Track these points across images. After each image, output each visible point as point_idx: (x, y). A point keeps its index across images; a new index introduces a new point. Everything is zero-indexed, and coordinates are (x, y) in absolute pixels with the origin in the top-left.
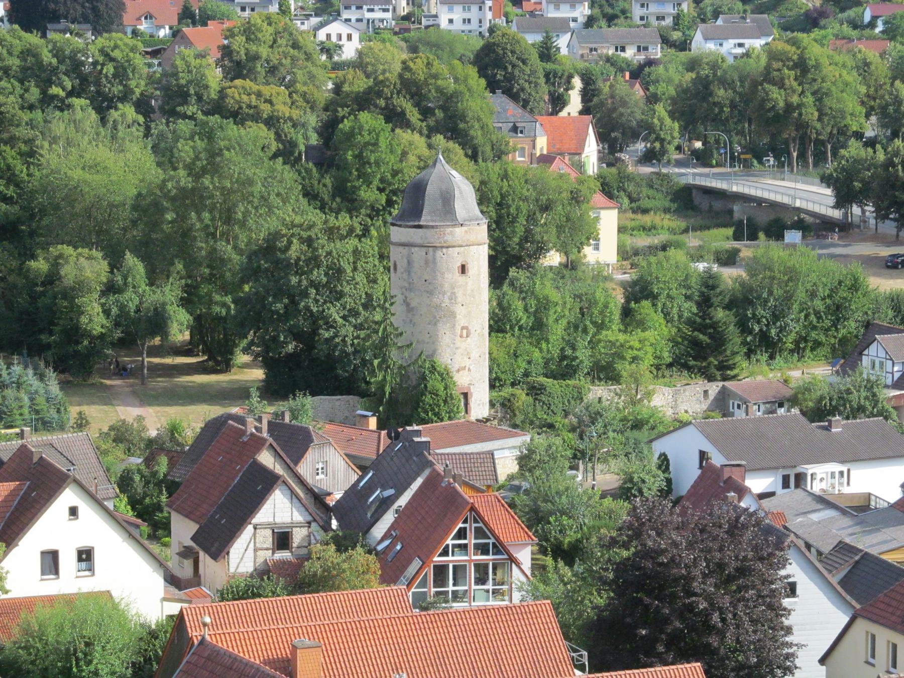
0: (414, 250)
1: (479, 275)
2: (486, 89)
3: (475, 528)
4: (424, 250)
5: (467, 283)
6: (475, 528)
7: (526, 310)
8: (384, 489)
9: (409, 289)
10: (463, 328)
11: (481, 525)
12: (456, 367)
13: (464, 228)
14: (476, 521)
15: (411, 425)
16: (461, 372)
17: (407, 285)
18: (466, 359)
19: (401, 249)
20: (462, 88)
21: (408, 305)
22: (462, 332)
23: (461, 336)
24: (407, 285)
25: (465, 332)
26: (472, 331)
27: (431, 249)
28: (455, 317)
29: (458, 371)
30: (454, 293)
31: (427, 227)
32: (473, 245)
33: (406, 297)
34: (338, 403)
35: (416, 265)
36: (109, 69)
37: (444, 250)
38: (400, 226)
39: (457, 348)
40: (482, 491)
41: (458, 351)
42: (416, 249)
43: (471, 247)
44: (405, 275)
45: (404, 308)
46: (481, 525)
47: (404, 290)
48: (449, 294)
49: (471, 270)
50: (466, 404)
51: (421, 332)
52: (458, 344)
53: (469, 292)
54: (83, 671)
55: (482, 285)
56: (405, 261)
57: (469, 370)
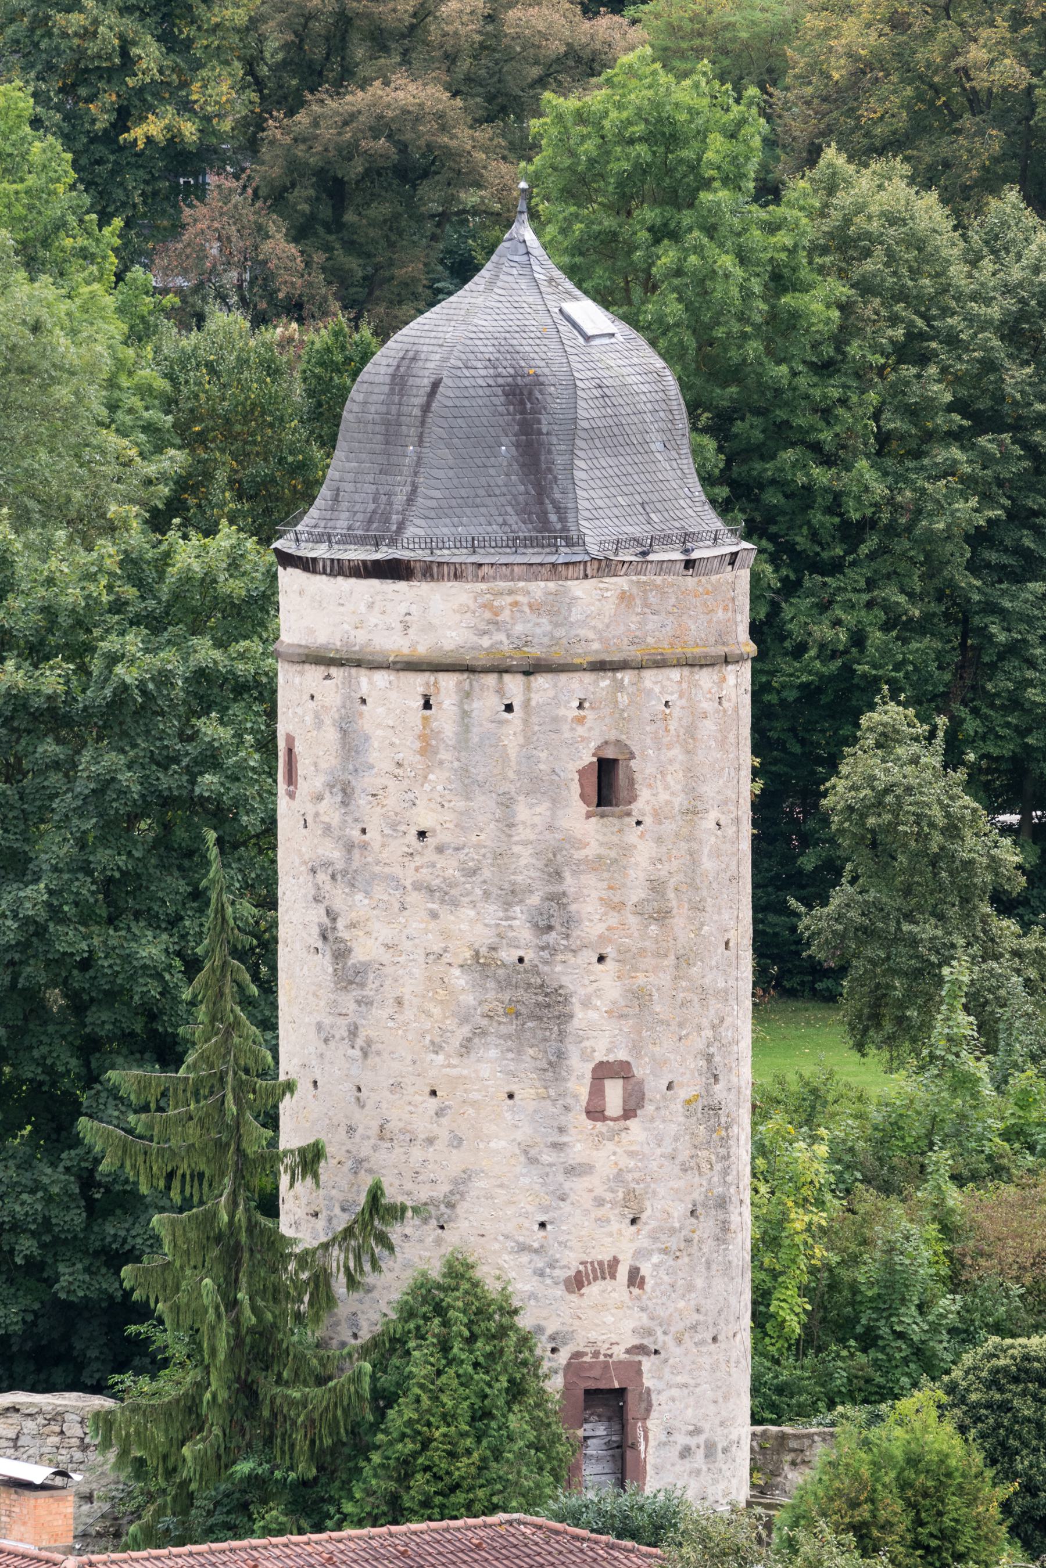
0: (373, 683)
2: (290, 1087)
4: (418, 682)
5: (627, 850)
7: (911, 595)
9: (347, 876)
10: (603, 1072)
16: (593, 1290)
17: (335, 854)
18: (619, 1225)
19: (314, 674)
21: (341, 954)
23: (595, 1113)
24: (335, 854)
25: (614, 1093)
26: (655, 1087)
27: (448, 682)
28: (566, 1017)
29: (577, 1283)
30: (557, 899)
31: (429, 572)
32: (660, 664)
37: (514, 684)
39: (571, 1171)
42: (381, 678)
43: (650, 677)
44: (329, 810)
45: (325, 962)
47: (322, 877)
48: (535, 900)
49: (653, 789)
51: (396, 1087)
52: (579, 1150)
53: (637, 893)
54: (75, 700)
56: (331, 735)
57: (635, 1279)
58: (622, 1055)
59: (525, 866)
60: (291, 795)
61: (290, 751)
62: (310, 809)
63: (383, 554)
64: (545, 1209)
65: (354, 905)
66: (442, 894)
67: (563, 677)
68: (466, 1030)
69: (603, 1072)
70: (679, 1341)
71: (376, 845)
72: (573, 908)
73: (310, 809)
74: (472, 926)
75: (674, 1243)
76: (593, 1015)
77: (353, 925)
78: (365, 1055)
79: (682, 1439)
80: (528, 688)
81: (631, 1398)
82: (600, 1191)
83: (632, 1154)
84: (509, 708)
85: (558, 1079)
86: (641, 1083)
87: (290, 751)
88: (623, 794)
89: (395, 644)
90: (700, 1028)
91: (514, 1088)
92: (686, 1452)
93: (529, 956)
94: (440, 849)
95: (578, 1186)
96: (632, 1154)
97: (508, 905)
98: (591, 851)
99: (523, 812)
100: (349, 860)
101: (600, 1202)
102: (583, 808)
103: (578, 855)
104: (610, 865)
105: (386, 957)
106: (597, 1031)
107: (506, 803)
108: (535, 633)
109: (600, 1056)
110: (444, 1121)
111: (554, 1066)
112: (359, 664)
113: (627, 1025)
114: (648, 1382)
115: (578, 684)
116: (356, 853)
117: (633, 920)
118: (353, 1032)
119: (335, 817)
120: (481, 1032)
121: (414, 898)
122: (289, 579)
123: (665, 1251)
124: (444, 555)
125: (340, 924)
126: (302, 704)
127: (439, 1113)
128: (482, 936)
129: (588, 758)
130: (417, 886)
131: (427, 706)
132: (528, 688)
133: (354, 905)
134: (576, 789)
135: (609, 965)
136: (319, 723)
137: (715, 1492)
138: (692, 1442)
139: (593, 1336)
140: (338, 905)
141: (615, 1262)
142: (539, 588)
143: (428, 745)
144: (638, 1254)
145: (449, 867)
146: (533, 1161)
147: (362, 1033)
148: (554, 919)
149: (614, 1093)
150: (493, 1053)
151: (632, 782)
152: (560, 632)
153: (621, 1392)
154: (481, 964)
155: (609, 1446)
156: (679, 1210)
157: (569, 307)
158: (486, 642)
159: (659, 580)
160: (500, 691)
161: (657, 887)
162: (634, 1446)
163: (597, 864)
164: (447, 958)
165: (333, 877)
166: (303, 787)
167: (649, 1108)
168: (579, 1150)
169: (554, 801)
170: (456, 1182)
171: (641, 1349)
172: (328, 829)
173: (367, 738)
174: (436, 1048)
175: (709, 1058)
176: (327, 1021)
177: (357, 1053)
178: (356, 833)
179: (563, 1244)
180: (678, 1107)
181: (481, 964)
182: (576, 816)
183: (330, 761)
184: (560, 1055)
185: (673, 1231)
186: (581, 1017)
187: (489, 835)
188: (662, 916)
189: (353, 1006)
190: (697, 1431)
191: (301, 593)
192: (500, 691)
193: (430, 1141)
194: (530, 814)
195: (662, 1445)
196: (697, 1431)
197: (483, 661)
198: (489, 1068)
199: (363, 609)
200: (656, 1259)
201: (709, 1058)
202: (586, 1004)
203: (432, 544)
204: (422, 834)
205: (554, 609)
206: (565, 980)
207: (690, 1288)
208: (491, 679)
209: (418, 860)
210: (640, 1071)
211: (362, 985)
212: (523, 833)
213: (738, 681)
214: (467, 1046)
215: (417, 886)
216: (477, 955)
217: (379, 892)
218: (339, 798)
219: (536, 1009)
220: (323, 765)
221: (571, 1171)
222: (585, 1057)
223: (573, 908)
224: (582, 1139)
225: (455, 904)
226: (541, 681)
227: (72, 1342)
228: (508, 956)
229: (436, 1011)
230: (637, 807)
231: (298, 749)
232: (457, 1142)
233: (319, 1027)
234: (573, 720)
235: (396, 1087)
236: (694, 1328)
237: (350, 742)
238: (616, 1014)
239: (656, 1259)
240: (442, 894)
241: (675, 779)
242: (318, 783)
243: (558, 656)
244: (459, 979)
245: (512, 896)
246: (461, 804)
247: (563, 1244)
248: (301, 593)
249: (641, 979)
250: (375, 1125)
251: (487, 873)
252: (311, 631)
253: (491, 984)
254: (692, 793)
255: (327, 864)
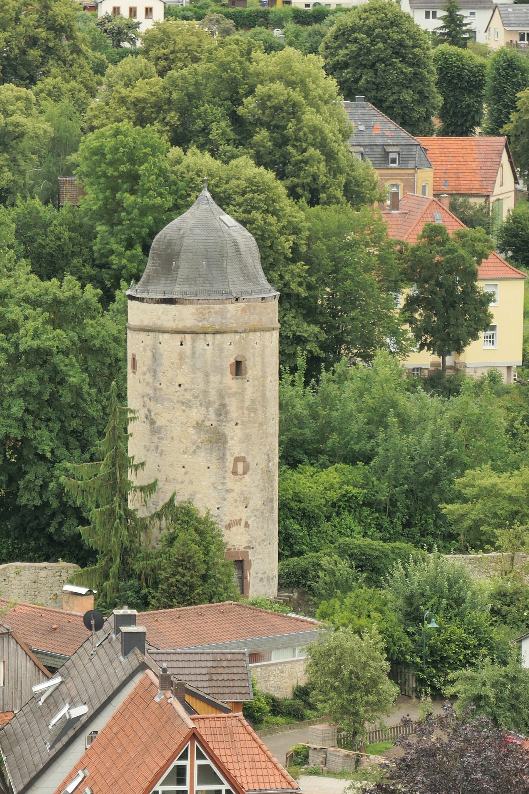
0: (162, 337)
1: (264, 377)
3: (200, 766)
4: (179, 337)
5: (244, 390)
6: (200, 766)
8: (73, 704)
9: (155, 399)
10: (237, 460)
11: (208, 762)
12: (227, 519)
13: (241, 305)
14: (200, 756)
15: (122, 608)
16: (234, 529)
17: (151, 392)
19: (142, 336)
20: (297, 95)
21: (152, 423)
22: (235, 466)
23: (235, 473)
24: (151, 392)
25: (240, 467)
26: (252, 465)
27: (188, 337)
28: (225, 442)
30: (224, 406)
32: (255, 330)
33: (149, 411)
34: (43, 573)
35: (165, 361)
36: (520, 229)
37: (209, 337)
38: (141, 300)
39: (227, 491)
40: (226, 710)
41: (230, 496)
42: (166, 336)
44: (148, 377)
45: (147, 426)
46: (208, 762)
47: (146, 399)
48: (216, 406)
49: (252, 370)
50: (242, 579)
51: (171, 465)
52: (230, 485)
53: (247, 404)
55: (268, 394)
56: (149, 354)
57: (247, 525)
58: (243, 455)
59: (213, 395)
60: (134, 373)
61: (134, 359)
62: (142, 377)
63: (167, 296)
64: (219, 503)
65: (156, 408)
66: (187, 404)
67: (225, 335)
68: (194, 447)
69: (237, 460)
70: (259, 545)
71: (164, 389)
72: (228, 408)
73: (142, 377)
74: (196, 414)
75: (258, 513)
76: (234, 442)
77: (157, 414)
78: (161, 455)
79: (260, 576)
80: (214, 338)
81: (245, 563)
82: (236, 498)
83: (246, 486)
84: (208, 345)
85: (224, 462)
86: (248, 463)
87: (134, 359)
88: (243, 372)
89: (170, 325)
90: (265, 445)
91: (209, 465)
92: (261, 580)
93: (214, 423)
94: (186, 390)
95: (229, 496)
96: (246, 486)
97: (207, 408)
98: (233, 390)
99: (212, 378)
100: (155, 394)
101: (236, 501)
102: (230, 376)
103: (230, 391)
104: (242, 392)
105: (168, 424)
106: (235, 447)
107: (207, 375)
108: (215, 321)
109: (236, 455)
110: (187, 476)
111: (222, 458)
112: (159, 331)
113: (244, 445)
114: (250, 558)
115: (228, 337)
116: (158, 391)
117: (246, 412)
118: (157, 448)
119: (151, 380)
120: (198, 447)
121: (178, 405)
122: (131, 304)
123: (256, 516)
124: (187, 297)
125: (152, 414)
126: (136, 345)
127: (186, 473)
128: (200, 417)
129: (233, 361)
130: (178, 402)
131: (182, 344)
132: (214, 338)
133: (156, 408)
134: (229, 371)
135: (239, 426)
136: (145, 350)
137: (269, 592)
138: (263, 576)
139: (234, 543)
140: (151, 408)
141: (241, 520)
142: (217, 307)
143: (181, 357)
144: (249, 517)
145: (188, 396)
146: (215, 488)
147: (160, 448)
148: (222, 411)
149: (240, 467)
150: (203, 454)
151: (246, 368)
152: (224, 321)
153: (242, 561)
154: (199, 426)
155: (238, 578)
156: (260, 503)
157: (221, 217)
158: (200, 324)
159: (254, 304)
160: (205, 340)
161: (253, 401)
162: (246, 578)
163: (234, 395)
164: (188, 424)
165: (150, 399)
166: (139, 370)
167: (251, 471)
168: (230, 485)
169: (222, 374)
170: (191, 495)
171: (248, 547)
172: (148, 383)
173: (161, 355)
174: (185, 453)
175: (268, 455)
176: (148, 444)
177: (158, 455)
178: (158, 385)
179: (225, 514)
180: (259, 471)
181: (199, 426)
182: (229, 380)
183: (148, 361)
184: (224, 455)
185: (258, 510)
186: (230, 443)
187: (201, 386)
188: (255, 411)
189: (156, 440)
190: (265, 573)
191: (138, 309)
192: (205, 340)
193: (182, 482)
194: (214, 379)
195: (254, 578)
196: (265, 573)
197: (201, 331)
198: (202, 459)
199: (160, 314)
200: (253, 518)
201: (268, 455)
202: (232, 439)
203: (184, 293)
204: (180, 385)
205: (222, 314)
206: (226, 431)
207: (263, 528)
208: (202, 336)
209: (179, 394)
210: (248, 460)
211: (160, 433)
212: (212, 385)
213: (276, 335)
214: (195, 452)
215: (178, 402)
216: (197, 424)
217: (166, 403)
218: (152, 374)
219: (217, 440)
220: (146, 363)
221: (227, 491)
222: (232, 455)
223: (228, 408)
224: (231, 482)
225: (191, 407)
226: (218, 336)
227: (42, 533)
228: (208, 423)
229: (184, 441)
230: (247, 376)
231: (137, 358)
232: (191, 482)
233: (145, 446)
234: (230, 348)
235: (171, 465)
236: (263, 540)
237: (155, 357)
238: (242, 442)
239: (253, 518)
240: (187, 404)
241: (259, 367)
242: (145, 369)
243: (224, 328)
244: (191, 431)
245: (209, 404)
246: (192, 375)
247: (225, 514)
248: (138, 309)
249: (248, 431)
250: (164, 477)
251: (201, 397)
252: (142, 321)
253: (202, 433)
254: (263, 371)
255: (148, 395)
